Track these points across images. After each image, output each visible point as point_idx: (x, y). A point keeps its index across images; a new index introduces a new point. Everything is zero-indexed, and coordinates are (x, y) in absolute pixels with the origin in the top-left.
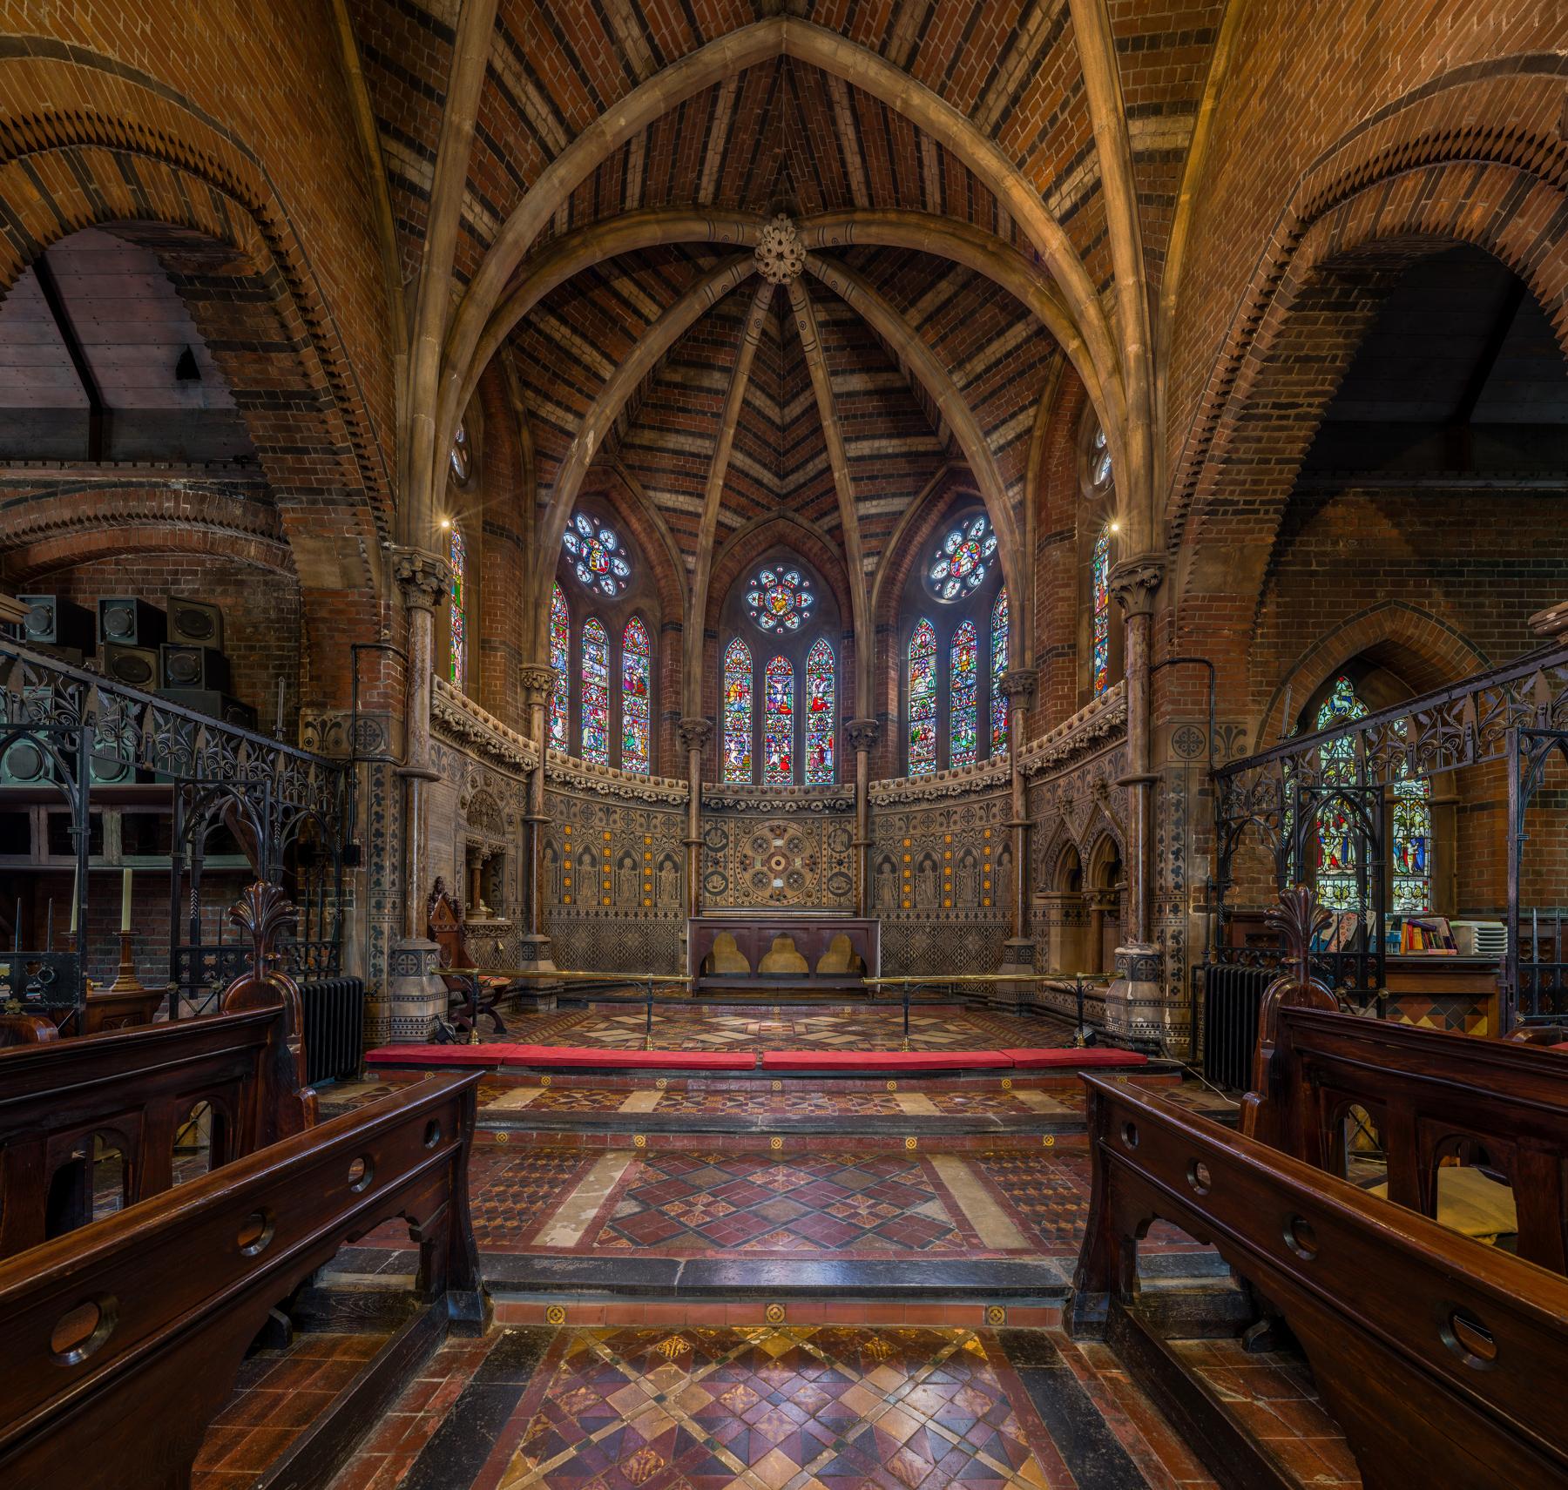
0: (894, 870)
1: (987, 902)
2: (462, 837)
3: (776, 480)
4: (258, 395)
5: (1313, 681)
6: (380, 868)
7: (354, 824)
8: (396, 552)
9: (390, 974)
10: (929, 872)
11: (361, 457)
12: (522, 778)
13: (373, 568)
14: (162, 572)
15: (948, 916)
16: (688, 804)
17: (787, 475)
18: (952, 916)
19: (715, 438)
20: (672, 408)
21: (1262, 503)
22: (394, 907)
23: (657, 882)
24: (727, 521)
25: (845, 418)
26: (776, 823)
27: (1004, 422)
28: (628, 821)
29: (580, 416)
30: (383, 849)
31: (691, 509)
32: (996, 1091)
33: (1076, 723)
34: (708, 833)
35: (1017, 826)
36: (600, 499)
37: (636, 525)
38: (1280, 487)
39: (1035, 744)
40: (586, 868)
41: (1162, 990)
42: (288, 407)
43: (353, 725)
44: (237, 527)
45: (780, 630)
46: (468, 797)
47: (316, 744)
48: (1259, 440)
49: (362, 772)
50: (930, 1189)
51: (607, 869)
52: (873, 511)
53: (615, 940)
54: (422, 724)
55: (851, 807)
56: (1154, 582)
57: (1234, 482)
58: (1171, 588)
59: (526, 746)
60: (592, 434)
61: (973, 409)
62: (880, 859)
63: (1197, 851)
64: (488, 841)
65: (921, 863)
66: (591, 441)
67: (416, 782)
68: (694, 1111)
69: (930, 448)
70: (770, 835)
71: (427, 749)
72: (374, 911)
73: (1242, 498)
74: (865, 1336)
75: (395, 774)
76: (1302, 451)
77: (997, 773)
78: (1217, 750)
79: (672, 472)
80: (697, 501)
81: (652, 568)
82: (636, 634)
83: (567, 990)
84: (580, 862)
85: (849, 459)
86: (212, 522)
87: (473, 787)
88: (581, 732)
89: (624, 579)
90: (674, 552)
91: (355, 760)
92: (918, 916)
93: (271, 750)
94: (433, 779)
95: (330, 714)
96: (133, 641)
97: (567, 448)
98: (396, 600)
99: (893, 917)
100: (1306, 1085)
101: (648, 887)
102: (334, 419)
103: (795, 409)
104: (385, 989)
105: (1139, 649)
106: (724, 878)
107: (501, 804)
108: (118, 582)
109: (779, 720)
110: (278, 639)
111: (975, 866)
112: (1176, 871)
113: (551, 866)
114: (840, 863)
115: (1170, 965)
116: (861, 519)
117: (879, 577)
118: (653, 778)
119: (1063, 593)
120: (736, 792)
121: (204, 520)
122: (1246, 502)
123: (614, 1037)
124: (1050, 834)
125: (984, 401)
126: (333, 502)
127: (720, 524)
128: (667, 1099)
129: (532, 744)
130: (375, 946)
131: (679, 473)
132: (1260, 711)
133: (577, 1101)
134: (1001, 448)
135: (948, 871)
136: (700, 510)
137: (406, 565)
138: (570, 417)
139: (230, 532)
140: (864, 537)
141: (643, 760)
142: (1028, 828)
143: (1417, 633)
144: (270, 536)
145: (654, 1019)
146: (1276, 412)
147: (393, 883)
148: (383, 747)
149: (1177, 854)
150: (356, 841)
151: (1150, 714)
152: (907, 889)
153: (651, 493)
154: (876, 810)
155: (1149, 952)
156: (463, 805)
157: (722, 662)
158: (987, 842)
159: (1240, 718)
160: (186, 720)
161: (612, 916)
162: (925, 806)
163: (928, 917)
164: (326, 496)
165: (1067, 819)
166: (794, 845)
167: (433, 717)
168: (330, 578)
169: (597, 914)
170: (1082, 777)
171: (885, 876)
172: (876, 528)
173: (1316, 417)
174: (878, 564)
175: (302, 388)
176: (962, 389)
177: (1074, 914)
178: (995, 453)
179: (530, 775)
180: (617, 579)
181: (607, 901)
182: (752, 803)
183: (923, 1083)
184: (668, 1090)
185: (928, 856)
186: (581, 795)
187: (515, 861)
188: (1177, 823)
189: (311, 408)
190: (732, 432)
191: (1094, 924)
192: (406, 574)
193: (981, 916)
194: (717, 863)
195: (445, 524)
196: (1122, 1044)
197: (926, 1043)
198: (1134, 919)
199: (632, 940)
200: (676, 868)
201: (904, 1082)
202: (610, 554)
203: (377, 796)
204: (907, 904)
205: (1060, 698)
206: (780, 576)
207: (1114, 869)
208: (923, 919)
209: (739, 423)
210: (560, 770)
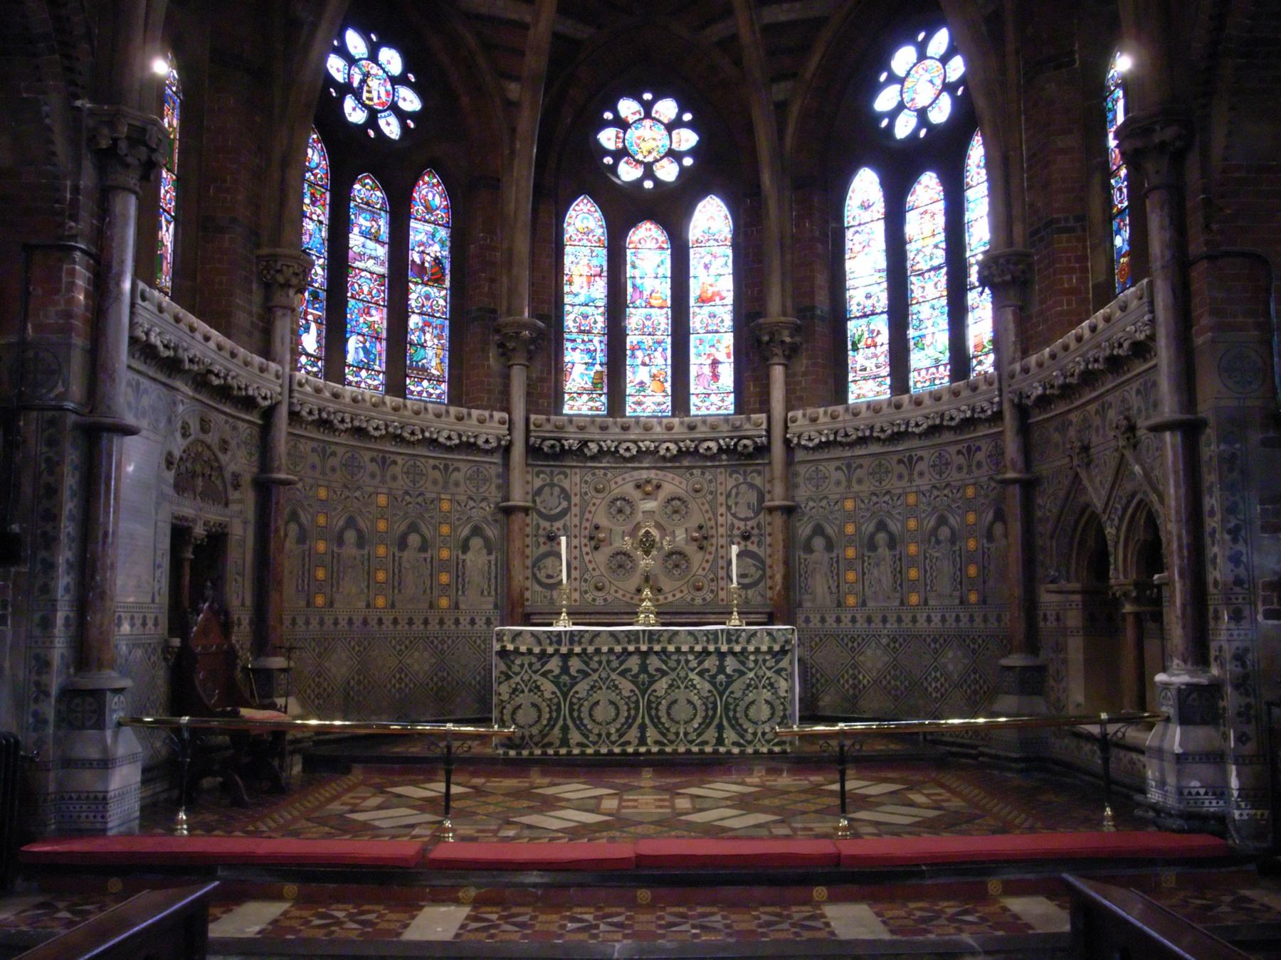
0: (830, 546)
8: (92, 113)
9: (57, 727)
12: (255, 418)
15: (914, 620)
16: (507, 450)
18: (922, 619)
23: (459, 571)
26: (644, 475)
28: (414, 473)
31: (514, 16)
34: (539, 492)
35: (1013, 481)
39: (1033, 360)
40: (350, 550)
41: (1225, 737)
45: (648, 184)
46: (177, 454)
52: (783, 17)
55: (763, 450)
56: (1178, 144)
62: (466, 532)
63: (1264, 529)
64: (202, 515)
65: (872, 536)
68: (516, 937)
70: (637, 495)
72: (37, 632)
77: (981, 402)
82: (430, 193)
83: (317, 743)
84: (340, 541)
87: (184, 435)
88: (345, 341)
89: (412, 115)
92: (869, 620)
99: (830, 620)
101: (444, 578)
107: (224, 458)
109: (648, 317)
112: (1235, 559)
115: (1231, 700)
116: (768, 29)
117: (795, 110)
118: (453, 410)
120: (582, 429)
123: (391, 818)
124: (1062, 494)
127: (556, 36)
128: (476, 919)
129: (273, 366)
130: (37, 684)
133: (339, 923)
135: (913, 549)
136: (528, 19)
137: (106, 131)
141: (439, 380)
145: (455, 790)
148: (60, 389)
149: (1234, 533)
150: (15, 528)
152: (851, 576)
154: (800, 455)
155: (1203, 680)
156: (169, 463)
157: (560, 232)
158: (912, 511)
162: (875, 448)
163: (884, 620)
165: (1083, 475)
166: (676, 506)
167: (133, 340)
169: (365, 622)
170: (1102, 412)
171: (815, 556)
177: (1101, 613)
179: (269, 414)
180: (402, 115)
181: (380, 602)
185: (882, 526)
186: (343, 439)
192: (104, 143)
193: (964, 619)
195: (161, 67)
197: (877, 824)
202: (395, 81)
203: (48, 460)
204: (851, 600)
206: (648, 107)
207: (1152, 556)
208: (877, 624)
210: (313, 403)
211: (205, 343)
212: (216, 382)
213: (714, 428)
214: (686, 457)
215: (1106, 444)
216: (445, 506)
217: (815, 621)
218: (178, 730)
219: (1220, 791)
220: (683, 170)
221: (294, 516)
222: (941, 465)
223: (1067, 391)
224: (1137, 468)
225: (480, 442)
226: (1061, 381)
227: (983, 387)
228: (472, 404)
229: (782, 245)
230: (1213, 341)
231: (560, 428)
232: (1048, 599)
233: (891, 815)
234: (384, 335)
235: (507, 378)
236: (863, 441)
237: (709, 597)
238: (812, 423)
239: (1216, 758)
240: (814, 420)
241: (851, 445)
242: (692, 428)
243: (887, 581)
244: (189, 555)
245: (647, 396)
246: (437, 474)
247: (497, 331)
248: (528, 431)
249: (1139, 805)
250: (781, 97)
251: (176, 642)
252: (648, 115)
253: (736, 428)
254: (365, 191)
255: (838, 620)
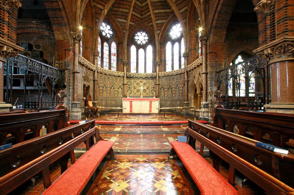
0: (164, 89)
1: (181, 95)
2: (83, 83)
3: (141, 16)
4: (51, 9)
5: (234, 56)
6: (70, 89)
7: (65, 81)
9: (71, 107)
10: (170, 90)
11: (67, 18)
13: (69, 36)
14: (30, 37)
15: (174, 98)
16: (124, 77)
17: (143, 15)
19: (129, 9)
20: (121, 4)
21: (223, 27)
22: (72, 96)
23: (118, 92)
24: (131, 24)
25: (152, 6)
26: (141, 80)
27: (182, 8)
28: (112, 80)
29: (104, 6)
30: (70, 85)
31: (124, 22)
32: (180, 127)
33: (195, 63)
35: (186, 81)
36: (108, 21)
37: (114, 25)
38: (226, 24)
39: (189, 66)
40: (105, 89)
41: (209, 110)
42: (56, 11)
43: (65, 64)
44: (44, 29)
46: (84, 76)
47: (58, 67)
48: (222, 17)
49: (66, 71)
50: (167, 141)
51: (108, 89)
52: (159, 22)
53: (110, 102)
54: (77, 63)
56: (206, 39)
57: (218, 23)
58: (209, 40)
59: (94, 66)
60: (106, 10)
61: (177, 6)
62: (119, 87)
64: (87, 84)
66: (106, 11)
67: (76, 73)
69: (169, 11)
70: (140, 83)
71: (78, 68)
73: (220, 26)
74: (155, 159)
75: (72, 72)
76: (229, 19)
77: (182, 71)
78: (217, 68)
79: (121, 15)
80: (125, 20)
81: (117, 32)
82: (114, 45)
84: (103, 88)
85: (154, 13)
86: (40, 28)
90: (121, 30)
91: (65, 70)
92: (168, 98)
93: (52, 68)
94: (79, 73)
95: (60, 62)
96: (27, 50)
97: (101, 12)
98: (72, 42)
99: (164, 98)
100: (220, 120)
102: (63, 12)
103: (144, 4)
104: (70, 110)
105: (205, 50)
106: (131, 91)
108: (22, 38)
110: (51, 48)
111: (179, 88)
112: (211, 89)
113: (98, 88)
114: (153, 88)
115: (210, 105)
116: (157, 24)
117: (160, 34)
119: (193, 39)
120: (133, 74)
121: (38, 28)
122: (221, 27)
123: (111, 119)
125: (179, 4)
126: (62, 26)
131: (122, 15)
132: (225, 61)
134: (182, 13)
135: (174, 89)
136: (126, 22)
137: (74, 36)
138: (102, 7)
139: (42, 30)
140: (157, 27)
142: (188, 81)
143: (250, 48)
144: (50, 31)
146: (224, 13)
147: (72, 91)
149: (211, 86)
150: (65, 84)
151: (207, 61)
152: (166, 93)
153: (117, 19)
154: (160, 78)
155: (207, 103)
156: (83, 77)
158: (174, 85)
159: (221, 62)
160: (41, 64)
161: (109, 98)
164: (61, 25)
165: (194, 80)
167: (79, 62)
168: (61, 38)
169: (107, 98)
172: (160, 25)
173: (231, 14)
174: (160, 32)
175: (59, 8)
176: (175, 2)
177: (196, 96)
178: (181, 13)
179: (94, 72)
180: (110, 35)
181: (108, 95)
182: (136, 76)
183: (167, 126)
184: (122, 127)
185: (170, 86)
186: (104, 75)
187: (92, 88)
188: (211, 81)
189: (60, 11)
190: (132, 8)
191: (199, 99)
192: (74, 37)
193: (180, 98)
194: (129, 88)
196: (202, 119)
198: (204, 97)
199: (113, 103)
200: (122, 89)
201: (164, 126)
203: (69, 76)
204: (166, 96)
205: (193, 58)
207: (202, 89)
209: (133, 7)
210: (100, 70)
211: (87, 62)
212: (88, 67)
213: (149, 74)
214: (146, 78)
215: (197, 76)
216: (116, 84)
217: (162, 98)
218: (86, 108)
219: (208, 116)
220: (140, 44)
221: (98, 84)
222: (177, 79)
223: (193, 70)
224: (200, 79)
225: (120, 76)
226: (192, 68)
227: (183, 69)
228: (120, 71)
229: (158, 52)
230: (210, 63)
231: (130, 74)
232: (189, 95)
233: (169, 120)
234: (108, 62)
235: (124, 68)
236: (168, 76)
237: (149, 95)
238: (161, 74)
239: (208, 112)
240: (162, 73)
241: (167, 77)
242: (147, 74)
243: (170, 93)
244: (85, 89)
245: (141, 71)
246: (115, 80)
247: (122, 62)
248: (126, 74)
249: (199, 118)
250: (158, 33)
251: (85, 98)
252: (141, 35)
253: (152, 74)
254: (105, 44)
255: (164, 98)
